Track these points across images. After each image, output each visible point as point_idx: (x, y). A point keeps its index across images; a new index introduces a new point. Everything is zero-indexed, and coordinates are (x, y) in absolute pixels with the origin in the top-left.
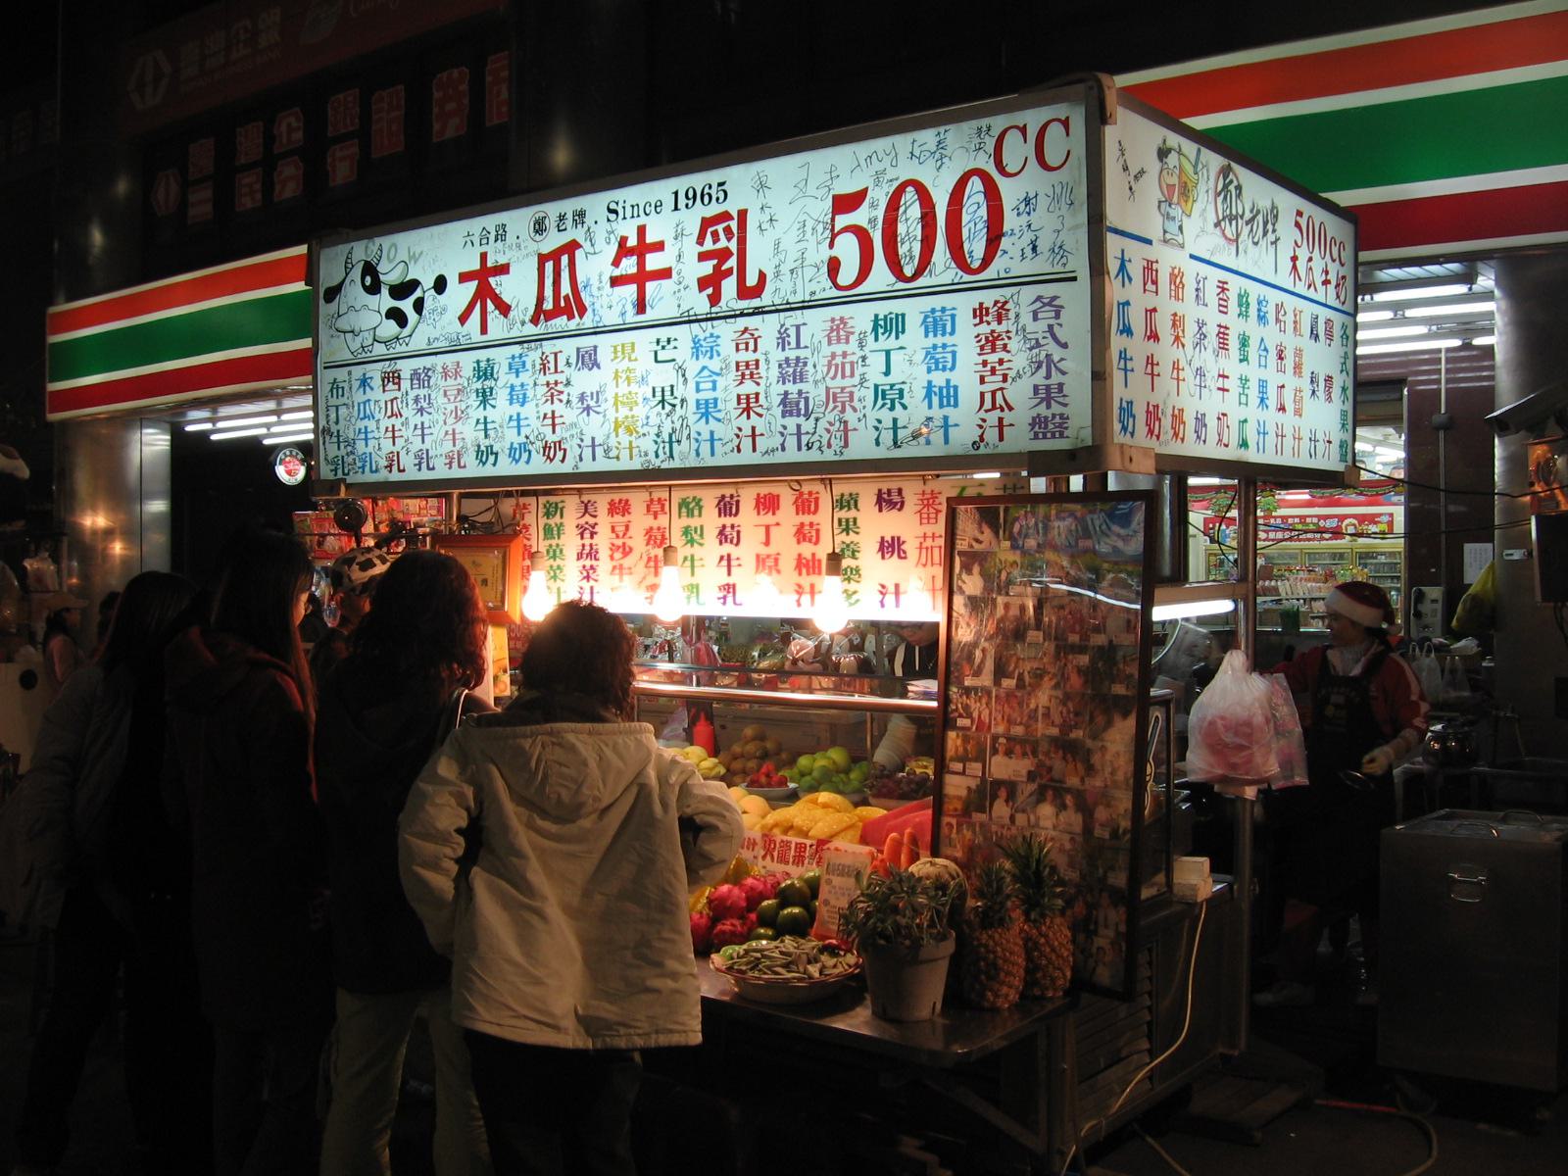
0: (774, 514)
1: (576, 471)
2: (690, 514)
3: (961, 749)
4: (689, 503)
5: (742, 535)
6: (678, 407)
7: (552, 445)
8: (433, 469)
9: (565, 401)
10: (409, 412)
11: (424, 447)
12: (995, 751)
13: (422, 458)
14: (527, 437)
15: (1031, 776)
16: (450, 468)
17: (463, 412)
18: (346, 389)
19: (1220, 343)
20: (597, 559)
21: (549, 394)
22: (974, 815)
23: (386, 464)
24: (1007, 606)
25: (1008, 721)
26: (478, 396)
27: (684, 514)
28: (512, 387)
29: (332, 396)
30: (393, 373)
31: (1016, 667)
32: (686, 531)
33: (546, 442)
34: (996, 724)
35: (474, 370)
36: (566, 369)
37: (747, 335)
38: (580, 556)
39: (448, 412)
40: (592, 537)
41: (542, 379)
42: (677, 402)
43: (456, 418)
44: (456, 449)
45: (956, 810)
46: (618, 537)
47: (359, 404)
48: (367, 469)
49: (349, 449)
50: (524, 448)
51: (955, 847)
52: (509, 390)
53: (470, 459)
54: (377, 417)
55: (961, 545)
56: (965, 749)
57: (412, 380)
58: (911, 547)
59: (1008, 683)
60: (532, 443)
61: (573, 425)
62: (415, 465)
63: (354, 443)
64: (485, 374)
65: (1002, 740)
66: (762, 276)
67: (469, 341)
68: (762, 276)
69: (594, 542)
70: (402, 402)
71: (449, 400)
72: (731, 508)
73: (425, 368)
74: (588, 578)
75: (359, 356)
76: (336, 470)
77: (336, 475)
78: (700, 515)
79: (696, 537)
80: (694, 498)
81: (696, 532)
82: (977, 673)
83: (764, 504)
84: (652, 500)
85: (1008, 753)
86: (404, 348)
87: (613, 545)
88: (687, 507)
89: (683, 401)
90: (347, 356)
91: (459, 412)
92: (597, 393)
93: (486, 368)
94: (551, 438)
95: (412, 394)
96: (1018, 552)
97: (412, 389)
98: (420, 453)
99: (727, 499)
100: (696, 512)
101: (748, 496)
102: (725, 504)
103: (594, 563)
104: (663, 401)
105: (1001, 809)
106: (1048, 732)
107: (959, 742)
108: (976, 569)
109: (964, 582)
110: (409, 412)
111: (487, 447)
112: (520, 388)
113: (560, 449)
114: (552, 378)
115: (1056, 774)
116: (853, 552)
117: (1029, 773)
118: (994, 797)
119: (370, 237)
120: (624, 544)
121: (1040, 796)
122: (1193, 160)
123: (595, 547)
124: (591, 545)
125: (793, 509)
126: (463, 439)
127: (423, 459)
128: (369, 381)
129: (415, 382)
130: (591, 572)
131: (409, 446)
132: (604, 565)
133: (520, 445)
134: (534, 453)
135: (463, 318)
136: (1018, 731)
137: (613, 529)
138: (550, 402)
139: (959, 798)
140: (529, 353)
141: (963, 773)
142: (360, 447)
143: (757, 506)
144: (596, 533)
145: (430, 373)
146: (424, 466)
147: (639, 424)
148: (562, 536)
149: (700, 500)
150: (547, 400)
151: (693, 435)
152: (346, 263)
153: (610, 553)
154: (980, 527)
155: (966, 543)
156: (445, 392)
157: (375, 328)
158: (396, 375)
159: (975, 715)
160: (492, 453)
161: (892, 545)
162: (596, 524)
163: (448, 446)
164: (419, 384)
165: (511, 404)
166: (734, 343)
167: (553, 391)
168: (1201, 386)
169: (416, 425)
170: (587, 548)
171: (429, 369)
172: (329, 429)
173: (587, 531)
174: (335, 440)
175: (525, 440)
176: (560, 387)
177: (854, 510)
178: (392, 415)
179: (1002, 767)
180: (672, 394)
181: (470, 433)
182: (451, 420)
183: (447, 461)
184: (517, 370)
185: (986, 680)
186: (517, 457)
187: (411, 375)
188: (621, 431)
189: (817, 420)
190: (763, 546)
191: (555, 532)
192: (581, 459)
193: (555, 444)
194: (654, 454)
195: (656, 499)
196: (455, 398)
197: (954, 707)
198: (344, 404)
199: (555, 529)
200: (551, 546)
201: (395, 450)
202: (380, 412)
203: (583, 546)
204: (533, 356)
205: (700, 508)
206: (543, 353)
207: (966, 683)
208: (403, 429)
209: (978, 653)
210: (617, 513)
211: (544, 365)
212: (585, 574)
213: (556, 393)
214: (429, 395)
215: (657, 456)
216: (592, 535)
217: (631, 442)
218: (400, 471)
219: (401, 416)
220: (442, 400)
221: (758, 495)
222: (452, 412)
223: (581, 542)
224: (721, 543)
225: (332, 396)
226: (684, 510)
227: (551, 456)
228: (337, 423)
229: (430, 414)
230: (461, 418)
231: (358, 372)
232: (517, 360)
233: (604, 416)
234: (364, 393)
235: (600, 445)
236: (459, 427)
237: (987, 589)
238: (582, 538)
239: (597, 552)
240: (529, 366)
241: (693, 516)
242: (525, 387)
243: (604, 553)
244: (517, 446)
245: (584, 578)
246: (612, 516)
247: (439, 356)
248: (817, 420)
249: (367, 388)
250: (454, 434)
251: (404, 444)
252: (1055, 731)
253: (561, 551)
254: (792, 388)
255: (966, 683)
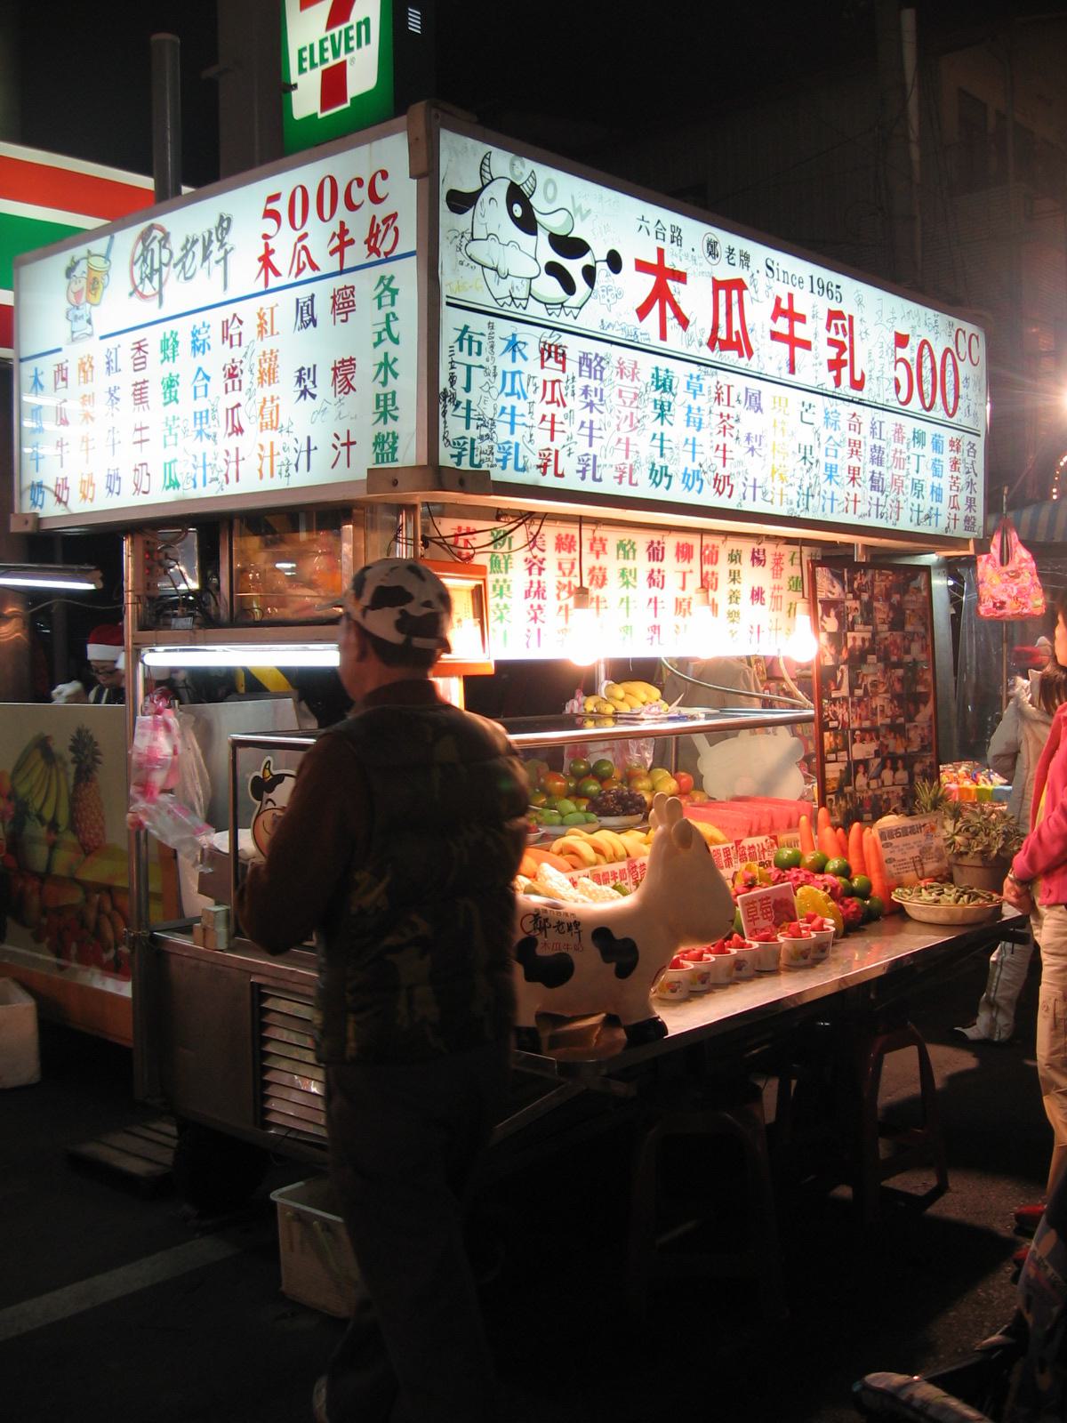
0: (689, 562)
1: (740, 509)
2: (626, 557)
3: (833, 744)
4: (626, 545)
5: (666, 579)
6: (814, 465)
7: (722, 478)
8: (600, 480)
9: (735, 437)
10: (575, 403)
11: (592, 451)
12: (854, 741)
13: (549, 460)
14: (701, 466)
15: (877, 754)
16: (620, 483)
17: (639, 421)
18: (485, 346)
19: (201, 413)
20: (544, 598)
21: (722, 426)
22: (845, 789)
23: (539, 462)
24: (854, 639)
25: (860, 718)
26: (655, 408)
27: (621, 556)
28: (690, 408)
29: (461, 350)
30: (557, 347)
31: (862, 682)
32: (623, 573)
33: (717, 474)
34: (853, 722)
35: (653, 377)
36: (736, 404)
37: (854, 419)
38: (527, 595)
39: (622, 416)
40: (540, 574)
41: (717, 409)
42: (813, 461)
43: (631, 425)
44: (628, 462)
45: (834, 788)
46: (564, 574)
47: (504, 373)
48: (510, 464)
49: (485, 431)
50: (697, 476)
51: (835, 815)
52: (686, 410)
53: (642, 476)
54: (531, 397)
55: (821, 595)
56: (836, 744)
57: (580, 363)
58: (767, 596)
59: (859, 692)
60: (705, 473)
61: (740, 462)
62: (578, 471)
63: (493, 424)
64: (664, 385)
65: (858, 733)
66: (863, 375)
67: (647, 342)
68: (863, 375)
69: (541, 578)
70: (567, 388)
71: (624, 402)
72: (658, 554)
73: (597, 355)
74: (535, 618)
75: (506, 307)
76: (459, 456)
77: (459, 463)
78: (634, 558)
79: (631, 579)
80: (630, 541)
81: (631, 574)
82: (838, 688)
83: (683, 553)
84: (594, 539)
85: (862, 740)
86: (569, 320)
87: (560, 583)
88: (624, 549)
89: (817, 461)
90: (486, 301)
91: (635, 421)
92: (761, 436)
93: (665, 380)
94: (722, 472)
95: (581, 383)
96: (858, 602)
97: (580, 375)
98: (585, 458)
99: (655, 545)
100: (631, 555)
101: (671, 542)
102: (653, 550)
103: (541, 602)
104: (805, 458)
105: (861, 780)
106: (884, 722)
107: (832, 739)
108: (832, 613)
109: (825, 622)
110: (575, 403)
111: (662, 467)
112: (696, 411)
113: (728, 484)
114: (726, 411)
115: (891, 749)
116: (737, 598)
117: (876, 751)
118: (856, 772)
119: (520, 153)
120: (570, 583)
121: (883, 766)
122: (397, 252)
123: (542, 585)
124: (539, 583)
125: (646, 556)
126: (637, 452)
127: (588, 466)
128: (521, 346)
129: (584, 368)
130: (538, 612)
131: (572, 446)
132: (551, 604)
133: (694, 472)
134: (705, 483)
135: (643, 312)
136: (867, 724)
137: (560, 566)
138: (722, 434)
139: (835, 779)
140: (705, 377)
141: (836, 761)
142: (502, 432)
143: (677, 554)
144: (544, 569)
145: (603, 364)
146: (589, 474)
147: (788, 474)
148: (509, 570)
149: (634, 543)
150: (720, 432)
151: (822, 493)
152: (483, 163)
153: (557, 592)
154: (832, 583)
155: (824, 594)
156: (620, 391)
157: (531, 279)
158: (560, 351)
159: (840, 717)
160: (666, 475)
161: (758, 594)
162: (544, 559)
163: (618, 457)
164: (590, 372)
165: (688, 425)
166: (848, 423)
167: (725, 423)
168: (808, 495)
169: (583, 423)
170: (535, 585)
171: (602, 359)
172: (454, 396)
173: (535, 567)
174: (463, 413)
175: (698, 468)
176: (731, 421)
177: (738, 564)
178: (553, 401)
179: (860, 751)
180: (811, 454)
181: (645, 450)
182: (625, 426)
183: (618, 474)
184: (695, 391)
185: (845, 691)
186: (690, 484)
187: (580, 358)
188: (776, 476)
189: (887, 496)
190: (680, 591)
191: (503, 566)
192: (744, 498)
193: (724, 477)
194: (796, 504)
195: (598, 537)
196: (632, 403)
197: (826, 714)
198: (481, 367)
199: (503, 561)
200: (497, 581)
201: (553, 446)
202: (535, 392)
203: (531, 582)
204: (710, 381)
205: (634, 551)
206: (718, 383)
207: (833, 696)
208: (567, 422)
209: (839, 675)
210: (564, 549)
211: (719, 395)
212: (533, 615)
213: (728, 427)
214: (602, 390)
215: (798, 506)
216: (541, 570)
217: (782, 490)
218: (556, 474)
219: (565, 405)
220: (616, 400)
221: (678, 544)
222: (627, 417)
223: (529, 578)
224: (650, 586)
225: (461, 350)
226: (621, 552)
227: (721, 489)
228: (468, 389)
229: (601, 413)
230: (636, 428)
231: (504, 328)
232: (695, 380)
233: (764, 460)
234: (514, 360)
235: (760, 487)
236: (633, 437)
237: (841, 625)
238: (530, 574)
239: (544, 591)
240: (705, 390)
241: (628, 558)
242: (701, 412)
243: (551, 591)
244: (691, 473)
245: (532, 619)
246: (560, 552)
247: (614, 346)
248: (887, 496)
249: (518, 354)
250: (628, 444)
251: (566, 443)
252: (888, 721)
253: (509, 586)
254: (877, 469)
255: (833, 696)
